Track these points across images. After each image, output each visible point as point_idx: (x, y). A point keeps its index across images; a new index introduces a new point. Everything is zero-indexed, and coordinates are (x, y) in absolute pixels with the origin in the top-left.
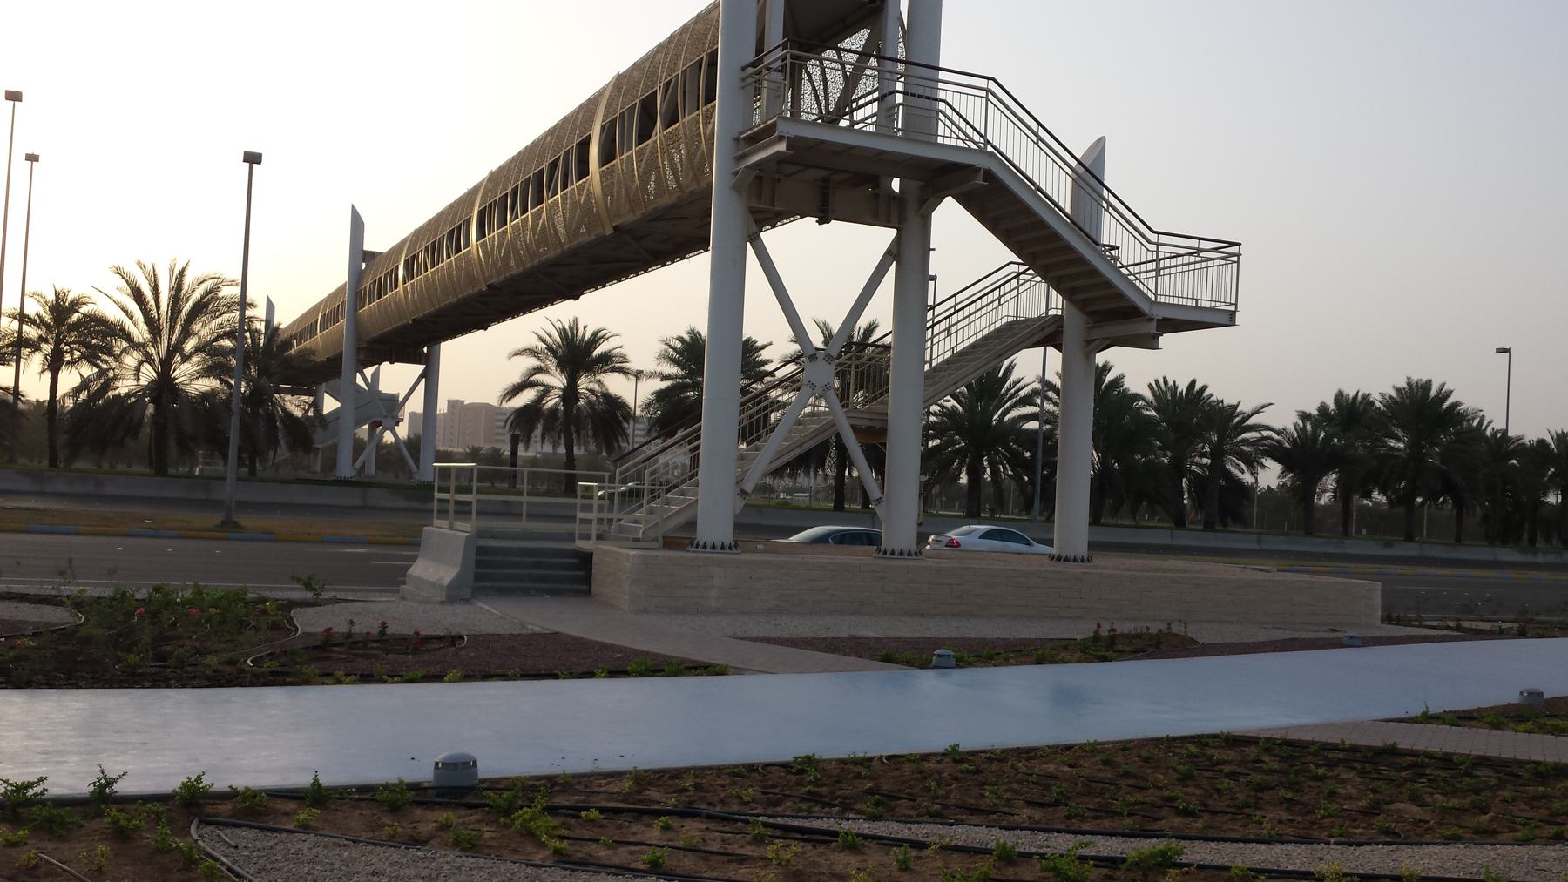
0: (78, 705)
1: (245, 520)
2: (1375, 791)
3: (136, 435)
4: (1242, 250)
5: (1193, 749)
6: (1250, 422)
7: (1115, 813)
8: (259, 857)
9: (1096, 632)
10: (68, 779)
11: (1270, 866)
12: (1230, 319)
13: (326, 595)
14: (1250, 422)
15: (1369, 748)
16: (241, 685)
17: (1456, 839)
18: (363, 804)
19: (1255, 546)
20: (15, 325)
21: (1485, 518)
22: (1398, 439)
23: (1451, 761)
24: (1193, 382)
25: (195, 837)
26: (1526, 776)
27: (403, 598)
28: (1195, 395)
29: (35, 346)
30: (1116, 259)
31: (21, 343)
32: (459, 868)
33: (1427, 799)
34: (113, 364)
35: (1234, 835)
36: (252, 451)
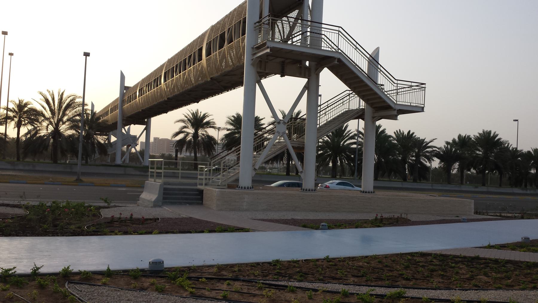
0: (27, 242)
1: (84, 179)
2: (472, 272)
3: (47, 149)
4: (426, 86)
5: (409, 257)
6: (429, 145)
7: (383, 279)
8: (89, 294)
9: (376, 217)
10: (23, 267)
11: (436, 298)
12: (422, 110)
13: (112, 204)
14: (429, 145)
15: (470, 257)
16: (83, 235)
17: (500, 288)
18: (125, 276)
19: (431, 188)
20: (5, 112)
21: (510, 178)
22: (480, 151)
23: (498, 261)
24: (409, 131)
25: (67, 287)
26: (524, 266)
27: (138, 206)
28: (410, 136)
29: (12, 119)
30: (383, 89)
31: (7, 118)
32: (157, 298)
33: (490, 274)
34: (39, 125)
35: (423, 287)
36: (87, 155)
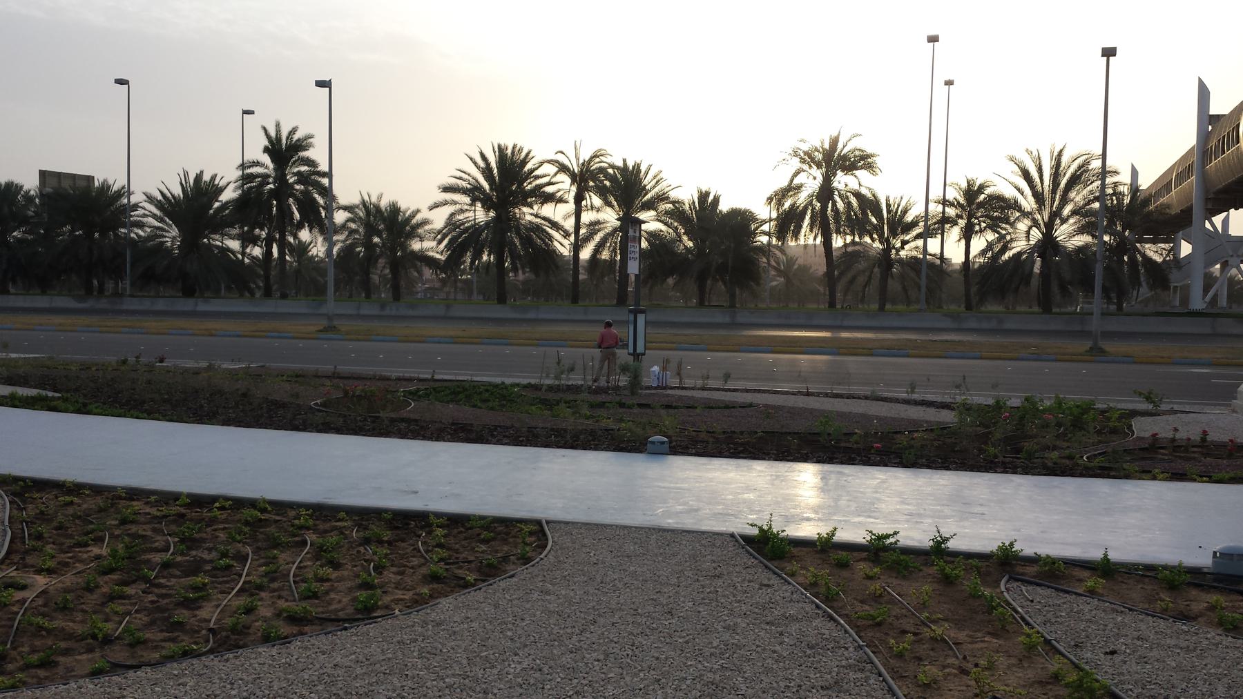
0: (942, 482)
1: (1109, 346)
3: (1028, 283)
8: (1048, 612)
10: (915, 535)
13: (1164, 407)
16: (1072, 475)
18: (1147, 580)
20: (940, 208)
25: (1003, 589)
27: (1234, 411)
29: (954, 223)
31: (945, 220)
32: (1217, 645)
34: (1010, 230)
36: (1117, 289)
